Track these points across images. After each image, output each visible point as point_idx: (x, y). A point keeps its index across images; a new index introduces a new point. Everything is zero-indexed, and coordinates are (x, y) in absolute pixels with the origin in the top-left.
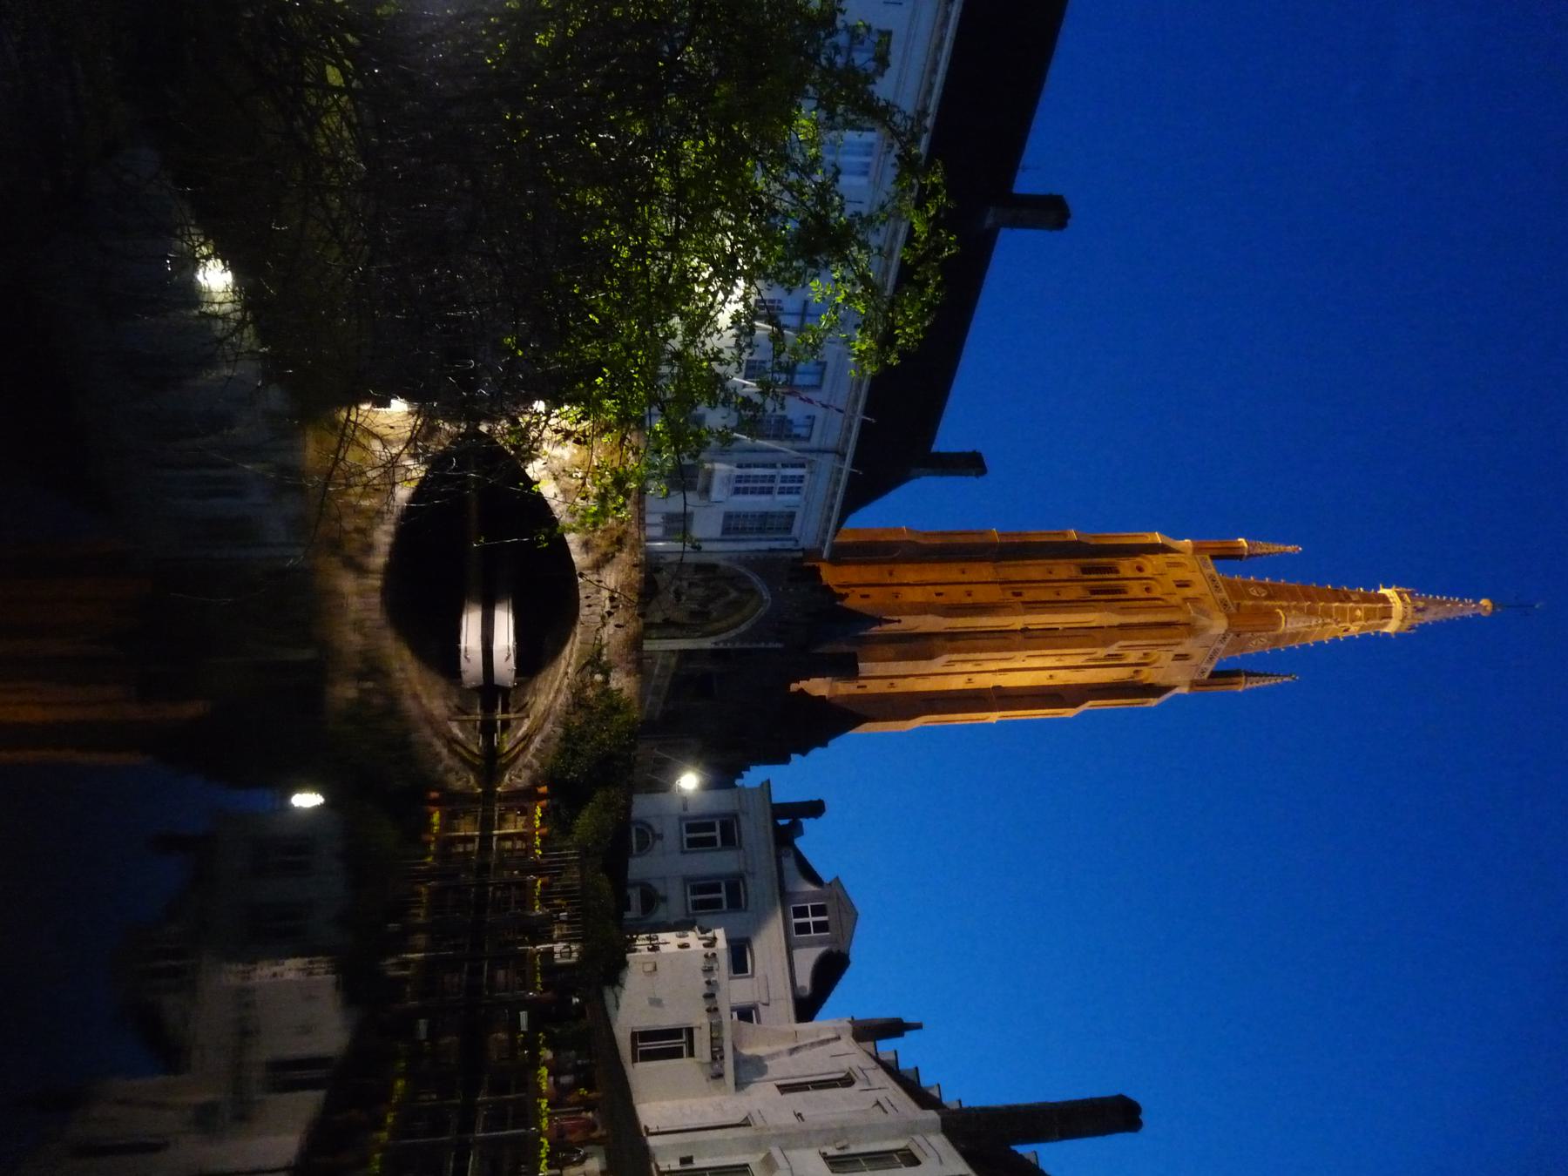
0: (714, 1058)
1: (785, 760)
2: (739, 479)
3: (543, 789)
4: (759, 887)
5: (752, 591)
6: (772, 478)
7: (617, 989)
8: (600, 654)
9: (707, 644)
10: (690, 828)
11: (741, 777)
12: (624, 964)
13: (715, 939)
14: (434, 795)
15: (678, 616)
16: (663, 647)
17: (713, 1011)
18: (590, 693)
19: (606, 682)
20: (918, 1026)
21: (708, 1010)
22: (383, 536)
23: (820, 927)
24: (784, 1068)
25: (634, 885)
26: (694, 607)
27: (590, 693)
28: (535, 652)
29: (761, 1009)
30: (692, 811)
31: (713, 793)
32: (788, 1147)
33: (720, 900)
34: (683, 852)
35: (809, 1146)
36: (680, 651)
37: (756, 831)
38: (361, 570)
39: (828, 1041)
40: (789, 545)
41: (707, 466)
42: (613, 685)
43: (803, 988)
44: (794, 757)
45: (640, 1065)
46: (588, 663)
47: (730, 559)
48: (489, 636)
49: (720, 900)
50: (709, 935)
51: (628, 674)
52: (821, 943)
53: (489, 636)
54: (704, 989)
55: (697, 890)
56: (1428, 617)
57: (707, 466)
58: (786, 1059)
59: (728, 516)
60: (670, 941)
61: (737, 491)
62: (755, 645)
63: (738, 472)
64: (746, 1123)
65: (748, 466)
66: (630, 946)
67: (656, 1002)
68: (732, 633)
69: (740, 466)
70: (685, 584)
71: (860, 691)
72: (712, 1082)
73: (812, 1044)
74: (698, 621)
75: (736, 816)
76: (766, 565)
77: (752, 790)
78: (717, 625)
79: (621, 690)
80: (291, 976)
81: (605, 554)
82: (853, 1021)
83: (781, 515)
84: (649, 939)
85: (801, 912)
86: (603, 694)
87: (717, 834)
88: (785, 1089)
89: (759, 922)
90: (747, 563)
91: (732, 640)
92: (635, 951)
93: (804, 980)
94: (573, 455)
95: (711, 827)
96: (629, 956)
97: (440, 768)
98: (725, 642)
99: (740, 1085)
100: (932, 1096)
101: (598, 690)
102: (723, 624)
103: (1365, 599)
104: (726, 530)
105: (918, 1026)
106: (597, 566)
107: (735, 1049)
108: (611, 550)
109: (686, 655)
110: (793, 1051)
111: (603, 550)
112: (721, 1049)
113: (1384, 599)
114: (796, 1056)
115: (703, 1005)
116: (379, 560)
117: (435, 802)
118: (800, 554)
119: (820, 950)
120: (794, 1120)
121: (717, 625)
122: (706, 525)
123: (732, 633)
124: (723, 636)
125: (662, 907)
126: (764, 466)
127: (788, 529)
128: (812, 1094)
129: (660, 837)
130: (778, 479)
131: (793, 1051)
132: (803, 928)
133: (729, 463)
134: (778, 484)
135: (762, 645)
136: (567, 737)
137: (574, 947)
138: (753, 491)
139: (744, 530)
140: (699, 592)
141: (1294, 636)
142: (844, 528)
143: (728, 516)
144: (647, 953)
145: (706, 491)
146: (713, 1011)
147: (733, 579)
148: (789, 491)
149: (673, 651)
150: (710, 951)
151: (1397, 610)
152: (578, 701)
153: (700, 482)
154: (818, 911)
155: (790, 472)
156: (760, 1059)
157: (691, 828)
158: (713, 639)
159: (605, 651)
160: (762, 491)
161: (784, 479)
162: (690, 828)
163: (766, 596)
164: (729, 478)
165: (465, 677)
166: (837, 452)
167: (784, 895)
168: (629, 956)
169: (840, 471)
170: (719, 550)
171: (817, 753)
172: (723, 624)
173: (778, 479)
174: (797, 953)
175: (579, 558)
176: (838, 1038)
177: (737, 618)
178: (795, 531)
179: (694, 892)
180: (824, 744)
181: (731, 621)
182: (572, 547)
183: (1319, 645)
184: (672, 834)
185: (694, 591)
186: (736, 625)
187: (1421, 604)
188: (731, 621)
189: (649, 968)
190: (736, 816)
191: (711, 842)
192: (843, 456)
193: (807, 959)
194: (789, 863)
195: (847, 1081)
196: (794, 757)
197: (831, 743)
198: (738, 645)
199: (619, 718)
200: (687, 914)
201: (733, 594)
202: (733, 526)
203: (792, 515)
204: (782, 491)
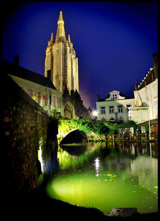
10: (102, 113)
15: (70, 114)
30: (100, 113)
31: (97, 110)
52: (118, 95)
55: (111, 112)
56: (62, 19)
58: (142, 100)
68: (73, 107)
74: (71, 112)
76: (64, 102)
78: (71, 109)
85: (114, 98)
87: (103, 109)
90: (64, 104)
95: (119, 109)
103: (59, 26)
109: (75, 114)
110: (141, 99)
113: (59, 24)
115: (138, 111)
119: (119, 96)
121: (71, 109)
123: (73, 107)
124: (73, 108)
129: (112, 117)
131: (141, 99)
132: (116, 98)
140: (67, 112)
141: (64, 35)
147: (66, 107)
151: (61, 22)
157: (111, 112)
177: (70, 106)
178: (59, 97)
183: (65, 32)
186: (71, 106)
187: (60, 19)
191: (104, 110)
201: (68, 107)
204: (55, 99)
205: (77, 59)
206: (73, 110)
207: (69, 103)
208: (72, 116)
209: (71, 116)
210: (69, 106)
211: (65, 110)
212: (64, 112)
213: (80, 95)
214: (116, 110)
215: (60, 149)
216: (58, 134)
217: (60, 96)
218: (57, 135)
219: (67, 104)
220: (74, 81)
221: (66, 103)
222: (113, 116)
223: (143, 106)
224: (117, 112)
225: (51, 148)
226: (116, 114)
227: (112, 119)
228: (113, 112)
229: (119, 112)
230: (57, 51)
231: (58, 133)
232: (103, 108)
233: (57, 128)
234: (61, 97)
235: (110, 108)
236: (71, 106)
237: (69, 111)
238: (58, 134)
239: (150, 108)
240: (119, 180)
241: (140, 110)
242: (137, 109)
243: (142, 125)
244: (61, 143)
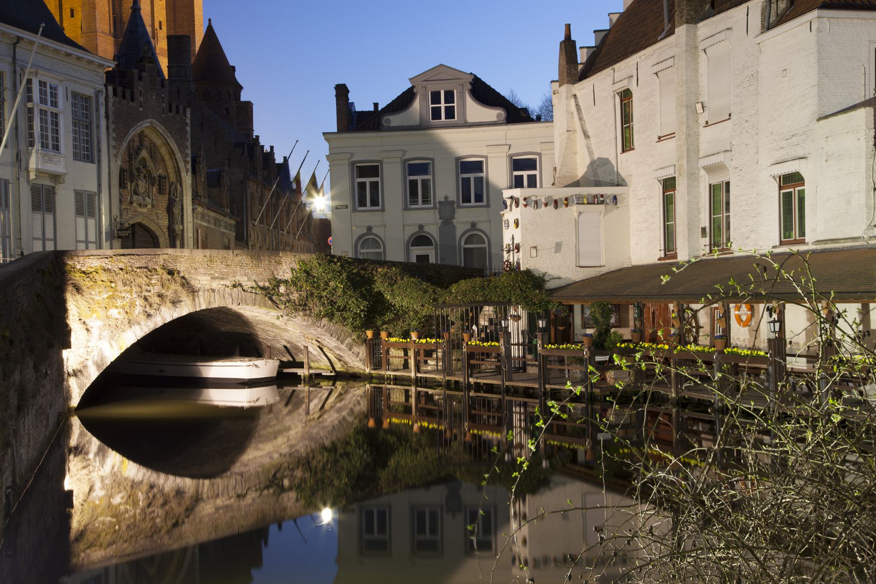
0: (602, 202)
1: (248, 107)
2: (44, 146)
3: (369, 334)
4: (414, 147)
5: (142, 136)
6: (43, 113)
7: (546, 278)
8: (263, 288)
9: (187, 179)
11: (263, 146)
12: (528, 272)
13: (512, 198)
14: (371, 423)
15: (163, 201)
16: (190, 219)
17: (567, 202)
18: (295, 296)
19: (286, 282)
20: (568, 27)
21: (567, 205)
22: (169, 482)
23: (449, 97)
24: (606, 144)
25: (408, 252)
26: (155, 189)
27: (295, 296)
28: (243, 342)
29: (512, 151)
30: (348, 202)
32: (697, 151)
33: (423, 181)
34: (383, 210)
35: (697, 135)
36: (193, 203)
37: (366, 147)
38: (197, 499)
39: (577, 105)
40: (102, 99)
41: (32, 176)
42: (288, 276)
43: (498, 115)
44: (244, 97)
46: (271, 299)
47: (116, 156)
48: (231, 383)
49: (423, 181)
50: (508, 202)
51: (279, 263)
53: (231, 383)
54: (551, 207)
57: (32, 176)
58: (593, 141)
59: (76, 157)
60: (510, 234)
61: (56, 148)
62: (189, 136)
63: (38, 145)
64: (669, 184)
65: (31, 135)
66: (514, 269)
67: (558, 247)
68: (178, 156)
69: (32, 144)
70: (135, 198)
71: (164, 27)
72: (619, 205)
73: (581, 119)
74: (167, 188)
75: (353, 164)
76: (121, 123)
77: (331, 148)
78: (171, 171)
79: (292, 269)
80: (525, 530)
81: (183, 285)
82: (561, 82)
83: (74, 105)
84: (509, 252)
85: (436, 114)
86: (295, 284)
87: (368, 180)
88: (627, 144)
89: (442, 148)
90: (120, 139)
91: (184, 155)
92: (518, 263)
93: (493, 114)
94: (98, 318)
95: (362, 186)
96: (523, 268)
97: (350, 419)
98: (186, 162)
99: (620, 183)
100: (618, 20)
101: (293, 289)
102: (170, 164)
104: (89, 159)
105: (568, 27)
106: (193, 291)
107: (577, 184)
108: (178, 279)
109: (195, 197)
110: (586, 136)
111: (180, 288)
112: (595, 196)
114: (590, 134)
115: (562, 209)
116: (187, 483)
117: (379, 422)
118: (110, 88)
120: (670, 144)
121: (171, 171)
122: (85, 177)
123: (178, 156)
124: (181, 165)
125: (426, 229)
126: (31, 119)
127: (87, 99)
128: (636, 124)
130: (44, 107)
131: (586, 136)
132: (450, 113)
133: (29, 154)
134: (48, 108)
135: (188, 129)
136: (330, 316)
137: (512, 312)
138: (57, 132)
139: (89, 142)
140: (142, 185)
142: (80, 42)
143: (76, 157)
144: (520, 254)
145: (56, 178)
146: (567, 202)
147: (132, 154)
148: (54, 95)
149: (193, 209)
150: (522, 202)
152: (302, 306)
153: (48, 183)
154: (436, 98)
155: (36, 95)
156: (592, 163)
158: (183, 174)
159: (261, 284)
160: (56, 124)
161: (43, 101)
162: (362, 203)
163: (146, 124)
164: (44, 155)
165: (271, 401)
166: (15, 45)
167: (422, 127)
168: (523, 268)
169: (43, 47)
170: (110, 163)
171: (239, 76)
172: (170, 164)
173: (44, 107)
174: (470, 119)
175: (184, 310)
176: (575, 96)
177: (164, 151)
178: (89, 92)
179: (416, 203)
180: (233, 68)
181: (167, 157)
182: (176, 315)
184: (368, 218)
185: (141, 190)
186: (172, 153)
188: (167, 157)
189: (534, 251)
190: (353, 164)
191: (375, 186)
192: (19, 39)
193: (475, 111)
194: (395, 120)
195: (626, 96)
196: (244, 97)
197: (231, 64)
198: (189, 152)
199: (318, 271)
200: (434, 208)
201: (144, 154)
202: (86, 152)
203: (75, 95)
204: (55, 104)
205: (267, 149)
206: (178, 172)
207: (150, 127)
208: (176, 211)
209: (169, 210)
210: (153, 150)
211: (126, 177)
212: (122, 185)
213: (233, 68)
214: (445, 186)
215: (81, 434)
216: (68, 346)
217: (92, 83)
218: (65, 353)
219: (142, 136)
220: (107, 185)
221: (133, 133)
222: (428, 219)
223: (598, 184)
224: (452, 197)
225: (10, 451)
226: (447, 210)
227: (421, 239)
228: (426, 200)
229: (467, 199)
230: (553, 184)
231: (73, 339)
232: (370, 170)
233: (62, 310)
234: (98, 93)
235: (411, 173)
236: (172, 153)
237: (151, 180)
238: (68, 346)
239: (615, 193)
240: (348, 340)
241: (574, 209)
242: (556, 202)
243: (577, 298)
244: (93, 395)
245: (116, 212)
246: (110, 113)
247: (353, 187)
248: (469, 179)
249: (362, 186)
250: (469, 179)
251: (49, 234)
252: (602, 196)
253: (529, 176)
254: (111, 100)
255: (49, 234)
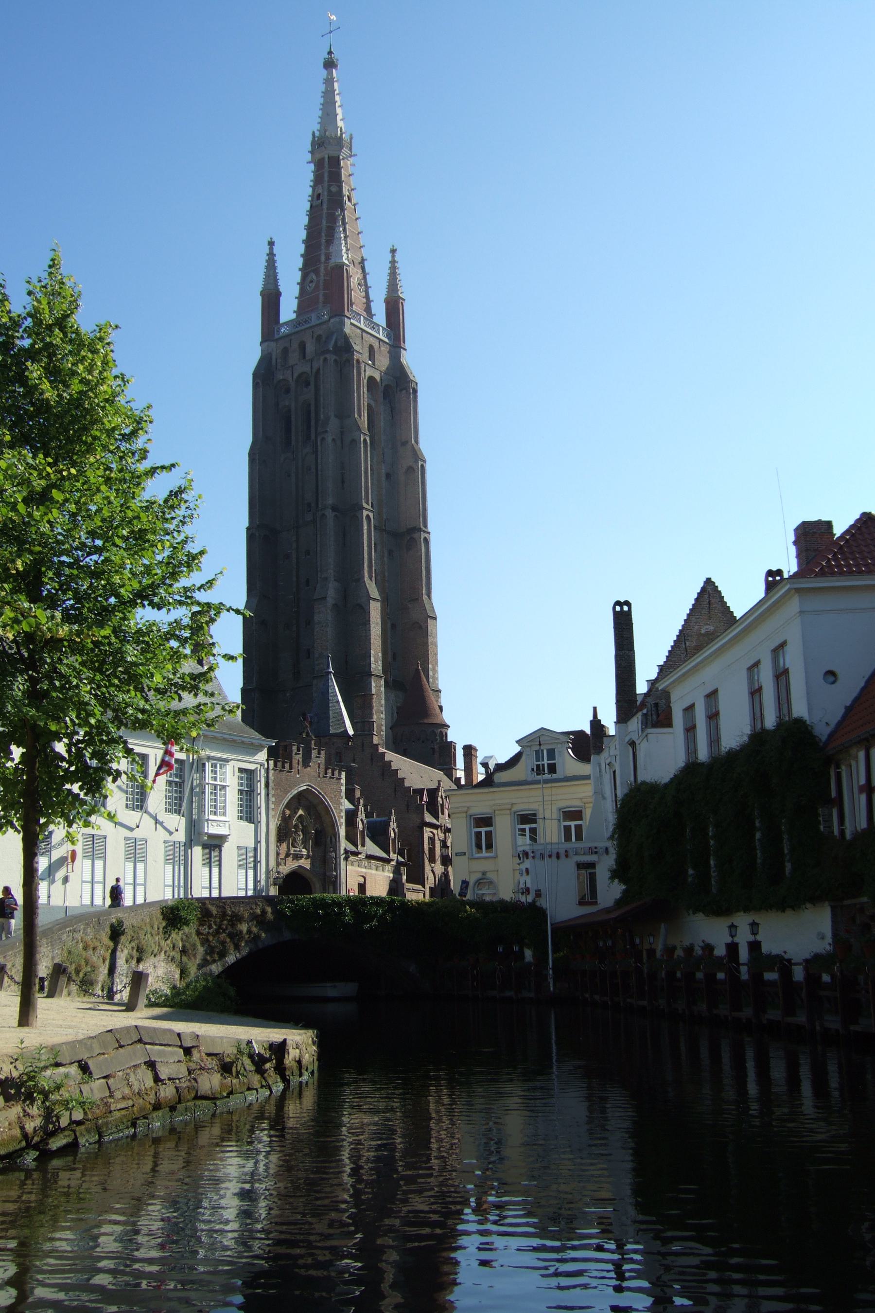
0: (596, 853)
20: (595, 709)
45: (599, 900)
95: (478, 834)
105: (595, 709)
118: (271, 763)
132: (552, 769)
232: (486, 821)
245: (272, 863)
246: (271, 782)
247: (559, 830)
248: (480, 832)
249: (478, 834)
250: (480, 832)
251: (215, 883)
252: (596, 848)
253: (576, 826)
254: (271, 773)
255: (215, 883)
